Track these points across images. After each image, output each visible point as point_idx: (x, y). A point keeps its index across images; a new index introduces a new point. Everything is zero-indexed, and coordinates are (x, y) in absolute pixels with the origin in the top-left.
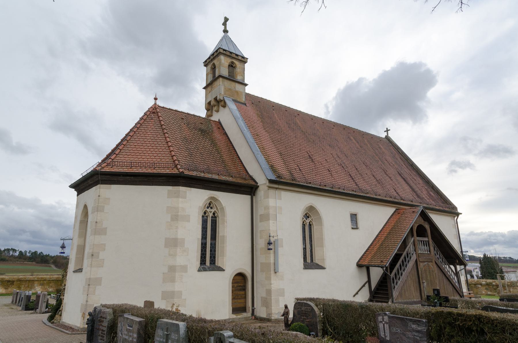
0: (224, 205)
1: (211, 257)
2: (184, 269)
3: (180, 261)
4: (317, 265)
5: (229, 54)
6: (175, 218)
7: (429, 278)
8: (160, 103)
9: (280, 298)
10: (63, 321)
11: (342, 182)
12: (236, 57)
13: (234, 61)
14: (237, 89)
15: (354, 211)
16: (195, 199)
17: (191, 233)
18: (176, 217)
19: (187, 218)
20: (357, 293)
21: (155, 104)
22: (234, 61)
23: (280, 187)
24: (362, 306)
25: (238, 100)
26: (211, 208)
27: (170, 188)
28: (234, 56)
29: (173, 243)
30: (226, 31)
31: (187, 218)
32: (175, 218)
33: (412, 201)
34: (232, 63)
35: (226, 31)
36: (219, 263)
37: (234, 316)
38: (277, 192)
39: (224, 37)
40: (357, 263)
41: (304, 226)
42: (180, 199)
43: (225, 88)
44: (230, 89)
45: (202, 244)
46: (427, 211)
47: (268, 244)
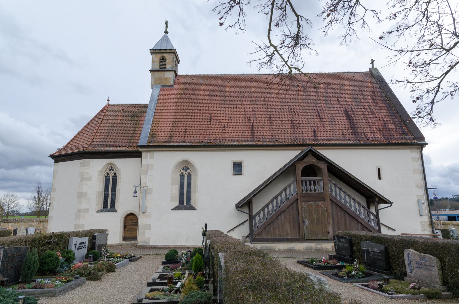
0: (119, 167)
1: (111, 203)
2: (87, 211)
3: (84, 206)
4: (192, 206)
5: (158, 51)
6: (83, 179)
7: (315, 216)
8: (111, 103)
9: (146, 231)
10: (72, 239)
11: (215, 134)
12: (165, 51)
13: (164, 55)
14: (165, 76)
15: (237, 159)
16: (97, 166)
17: (95, 187)
18: (84, 179)
19: (89, 179)
20: (232, 229)
21: (108, 104)
22: (164, 55)
23: (150, 149)
24: (238, 242)
25: (167, 84)
26: (113, 170)
27: (81, 160)
28: (163, 51)
29: (81, 195)
30: (166, 32)
31: (89, 179)
32: (83, 179)
33: (295, 140)
34: (163, 57)
35: (166, 32)
36: (192, 203)
37: (124, 242)
38: (151, 153)
39: (164, 36)
40: (236, 205)
41: (182, 176)
42: (86, 167)
43: (155, 79)
44: (160, 78)
45: (105, 194)
46: (314, 148)
47: (134, 192)
